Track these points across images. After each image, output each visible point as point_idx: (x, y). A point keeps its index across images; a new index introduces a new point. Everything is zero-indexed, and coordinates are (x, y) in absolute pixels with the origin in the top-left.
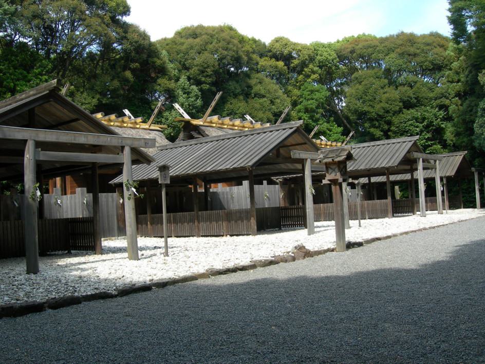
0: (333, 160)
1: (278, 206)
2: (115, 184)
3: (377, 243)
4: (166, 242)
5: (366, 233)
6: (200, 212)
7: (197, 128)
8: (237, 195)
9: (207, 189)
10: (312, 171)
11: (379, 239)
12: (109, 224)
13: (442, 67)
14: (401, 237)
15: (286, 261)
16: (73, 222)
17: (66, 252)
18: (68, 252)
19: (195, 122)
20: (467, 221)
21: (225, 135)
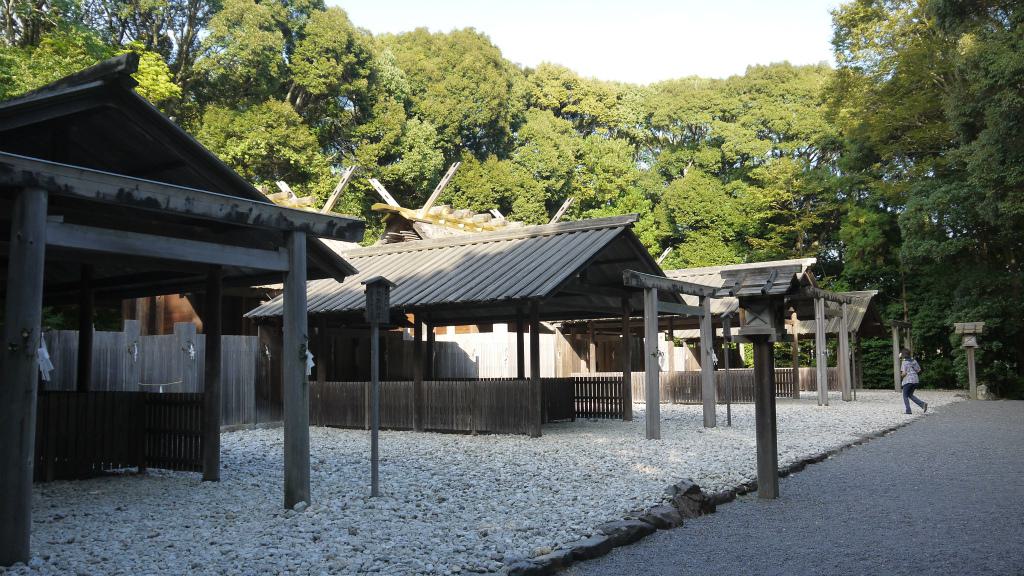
0: (763, 291)
1: (553, 376)
2: (256, 319)
3: (809, 467)
4: (297, 451)
5: (50, 522)
6: (425, 384)
7: (408, 225)
8: (492, 352)
9: (431, 335)
10: (659, 313)
11: (811, 461)
12: (238, 401)
13: (1016, 188)
14: (860, 448)
15: (743, 493)
16: (147, 402)
17: (135, 470)
18: (140, 472)
19: (407, 213)
20: (908, 427)
21: (448, 240)
